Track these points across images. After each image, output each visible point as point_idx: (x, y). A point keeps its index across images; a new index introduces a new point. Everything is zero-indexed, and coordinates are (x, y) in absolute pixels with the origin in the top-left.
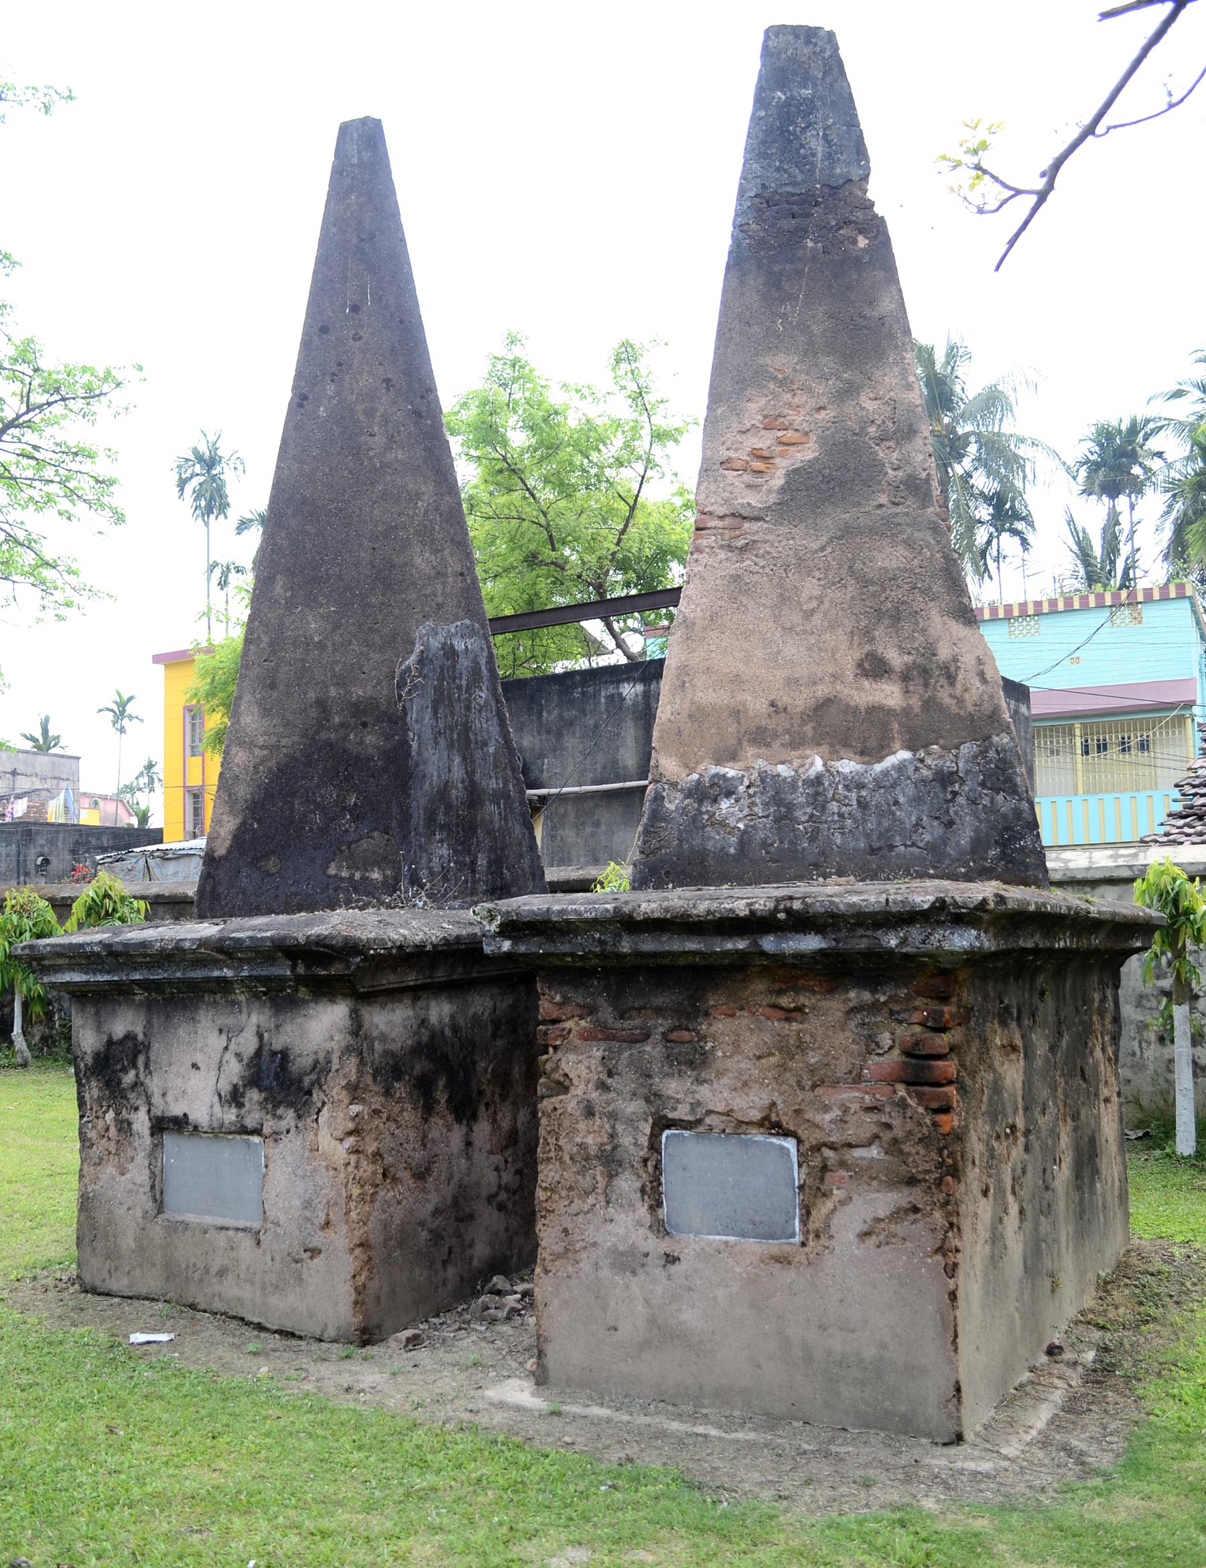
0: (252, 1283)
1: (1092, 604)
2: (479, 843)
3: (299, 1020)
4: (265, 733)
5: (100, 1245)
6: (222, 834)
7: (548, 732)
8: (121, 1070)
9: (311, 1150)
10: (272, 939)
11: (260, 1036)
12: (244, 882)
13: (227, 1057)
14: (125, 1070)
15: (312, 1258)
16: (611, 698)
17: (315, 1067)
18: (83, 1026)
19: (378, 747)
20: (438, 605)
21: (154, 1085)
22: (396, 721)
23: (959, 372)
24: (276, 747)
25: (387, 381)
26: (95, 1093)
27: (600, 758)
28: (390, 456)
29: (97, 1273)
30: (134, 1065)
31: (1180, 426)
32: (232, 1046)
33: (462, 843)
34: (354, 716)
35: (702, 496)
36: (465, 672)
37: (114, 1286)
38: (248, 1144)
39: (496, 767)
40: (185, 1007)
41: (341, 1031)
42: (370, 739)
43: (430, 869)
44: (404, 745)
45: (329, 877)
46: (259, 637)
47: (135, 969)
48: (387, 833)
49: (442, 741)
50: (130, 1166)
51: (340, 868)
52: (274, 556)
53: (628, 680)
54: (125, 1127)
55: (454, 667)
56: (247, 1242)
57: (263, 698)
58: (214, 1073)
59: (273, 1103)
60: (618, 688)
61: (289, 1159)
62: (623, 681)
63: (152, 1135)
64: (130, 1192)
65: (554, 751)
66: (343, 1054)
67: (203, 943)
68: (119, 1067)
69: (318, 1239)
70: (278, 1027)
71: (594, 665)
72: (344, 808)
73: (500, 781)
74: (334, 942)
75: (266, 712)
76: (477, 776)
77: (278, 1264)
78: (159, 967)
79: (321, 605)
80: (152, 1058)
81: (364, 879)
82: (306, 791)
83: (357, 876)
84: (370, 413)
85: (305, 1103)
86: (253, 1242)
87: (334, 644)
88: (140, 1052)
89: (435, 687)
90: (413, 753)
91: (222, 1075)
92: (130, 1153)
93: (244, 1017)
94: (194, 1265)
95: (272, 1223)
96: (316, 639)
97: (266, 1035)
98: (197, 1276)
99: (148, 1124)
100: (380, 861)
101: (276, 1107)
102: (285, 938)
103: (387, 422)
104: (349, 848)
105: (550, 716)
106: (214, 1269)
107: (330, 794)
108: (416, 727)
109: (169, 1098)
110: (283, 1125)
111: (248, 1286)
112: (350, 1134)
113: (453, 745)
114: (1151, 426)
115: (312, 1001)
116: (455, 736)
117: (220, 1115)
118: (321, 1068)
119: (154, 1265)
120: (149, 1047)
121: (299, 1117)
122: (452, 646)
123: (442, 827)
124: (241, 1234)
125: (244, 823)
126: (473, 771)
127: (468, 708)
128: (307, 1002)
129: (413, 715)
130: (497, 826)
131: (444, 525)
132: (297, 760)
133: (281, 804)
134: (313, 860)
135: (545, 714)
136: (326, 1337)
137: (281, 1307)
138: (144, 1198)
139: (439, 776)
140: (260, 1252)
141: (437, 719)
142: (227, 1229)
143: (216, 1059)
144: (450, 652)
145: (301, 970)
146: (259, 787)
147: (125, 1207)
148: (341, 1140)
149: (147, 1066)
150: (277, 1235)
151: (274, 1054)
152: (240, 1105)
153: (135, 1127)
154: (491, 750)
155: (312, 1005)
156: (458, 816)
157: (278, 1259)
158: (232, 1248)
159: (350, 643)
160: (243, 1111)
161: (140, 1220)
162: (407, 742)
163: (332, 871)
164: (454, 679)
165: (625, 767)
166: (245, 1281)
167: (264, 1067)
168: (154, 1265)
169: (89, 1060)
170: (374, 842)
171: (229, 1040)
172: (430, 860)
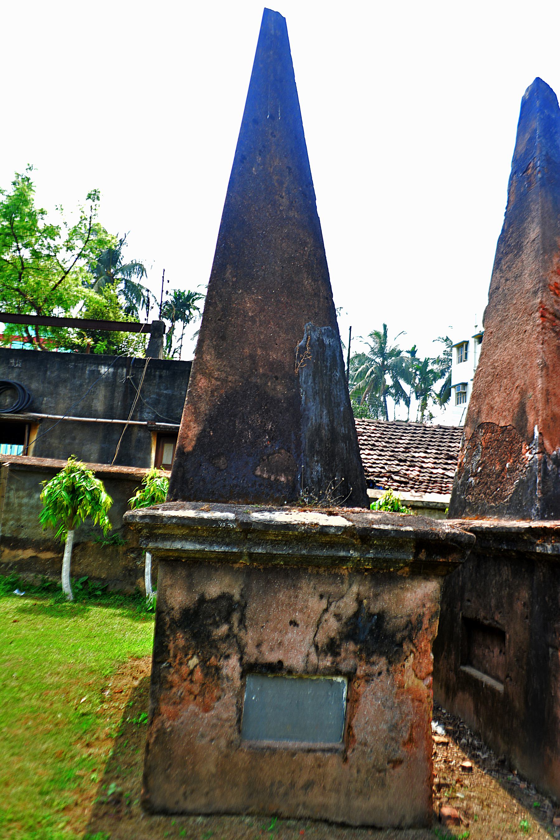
0: (338, 791)
2: (337, 466)
3: (396, 592)
4: (218, 370)
5: (175, 773)
6: (190, 435)
7: (49, 383)
10: (415, 533)
11: (359, 602)
12: (204, 473)
13: (326, 616)
14: (217, 625)
15: (394, 768)
16: (92, 372)
17: (407, 626)
18: (171, 586)
19: (283, 394)
20: (316, 313)
21: (249, 638)
22: (294, 380)
23: (122, 251)
24: (224, 381)
25: (289, 168)
26: (181, 642)
27: (81, 403)
28: (291, 214)
29: (168, 792)
30: (227, 620)
32: (332, 608)
33: (328, 465)
34: (271, 371)
35: (544, 299)
36: (329, 358)
37: (189, 806)
38: (332, 683)
39: (344, 420)
40: (287, 576)
41: (431, 601)
43: (312, 478)
44: (298, 395)
45: (256, 476)
46: (215, 303)
48: (289, 452)
49: (317, 398)
50: (216, 704)
51: (262, 471)
52: (226, 252)
53: (105, 365)
54: (213, 673)
55: (324, 353)
56: (334, 761)
57: (217, 345)
59: (366, 653)
60: (98, 367)
62: (102, 364)
64: (214, 726)
65: (52, 394)
70: (376, 596)
71: (12, 348)
72: (265, 430)
73: (346, 429)
77: (363, 775)
78: (285, 544)
79: (253, 293)
82: (243, 414)
83: (273, 478)
84: (281, 183)
86: (341, 759)
87: (260, 321)
88: (234, 610)
89: (314, 363)
90: (303, 402)
91: (321, 631)
92: (216, 693)
93: (345, 587)
94: (280, 782)
95: (360, 743)
96: (250, 314)
97: (365, 601)
98: (282, 790)
99: (238, 669)
100: (286, 470)
101: (369, 655)
103: (289, 193)
104: (268, 457)
105: (52, 374)
106: (301, 782)
107: (256, 419)
109: (264, 648)
110: (376, 668)
111: (333, 794)
113: (323, 402)
114: (197, 296)
115: (408, 578)
116: (324, 397)
117: (315, 661)
118: (413, 627)
121: (390, 663)
122: (323, 340)
123: (318, 453)
124: (328, 755)
125: (204, 430)
126: (333, 421)
127: (330, 380)
130: (345, 457)
131: (318, 266)
132: (238, 393)
133: (227, 421)
134: (247, 463)
135: (48, 373)
136: (403, 824)
138: (230, 731)
139: (316, 420)
140: (346, 767)
141: (315, 384)
143: (315, 618)
146: (214, 406)
147: (208, 739)
150: (364, 753)
151: (371, 615)
153: (224, 672)
154: (342, 409)
156: (326, 447)
158: (319, 766)
159: (269, 323)
160: (339, 659)
164: (324, 361)
165: (96, 410)
167: (361, 625)
169: (177, 615)
170: (281, 457)
171: (329, 604)
172: (312, 473)
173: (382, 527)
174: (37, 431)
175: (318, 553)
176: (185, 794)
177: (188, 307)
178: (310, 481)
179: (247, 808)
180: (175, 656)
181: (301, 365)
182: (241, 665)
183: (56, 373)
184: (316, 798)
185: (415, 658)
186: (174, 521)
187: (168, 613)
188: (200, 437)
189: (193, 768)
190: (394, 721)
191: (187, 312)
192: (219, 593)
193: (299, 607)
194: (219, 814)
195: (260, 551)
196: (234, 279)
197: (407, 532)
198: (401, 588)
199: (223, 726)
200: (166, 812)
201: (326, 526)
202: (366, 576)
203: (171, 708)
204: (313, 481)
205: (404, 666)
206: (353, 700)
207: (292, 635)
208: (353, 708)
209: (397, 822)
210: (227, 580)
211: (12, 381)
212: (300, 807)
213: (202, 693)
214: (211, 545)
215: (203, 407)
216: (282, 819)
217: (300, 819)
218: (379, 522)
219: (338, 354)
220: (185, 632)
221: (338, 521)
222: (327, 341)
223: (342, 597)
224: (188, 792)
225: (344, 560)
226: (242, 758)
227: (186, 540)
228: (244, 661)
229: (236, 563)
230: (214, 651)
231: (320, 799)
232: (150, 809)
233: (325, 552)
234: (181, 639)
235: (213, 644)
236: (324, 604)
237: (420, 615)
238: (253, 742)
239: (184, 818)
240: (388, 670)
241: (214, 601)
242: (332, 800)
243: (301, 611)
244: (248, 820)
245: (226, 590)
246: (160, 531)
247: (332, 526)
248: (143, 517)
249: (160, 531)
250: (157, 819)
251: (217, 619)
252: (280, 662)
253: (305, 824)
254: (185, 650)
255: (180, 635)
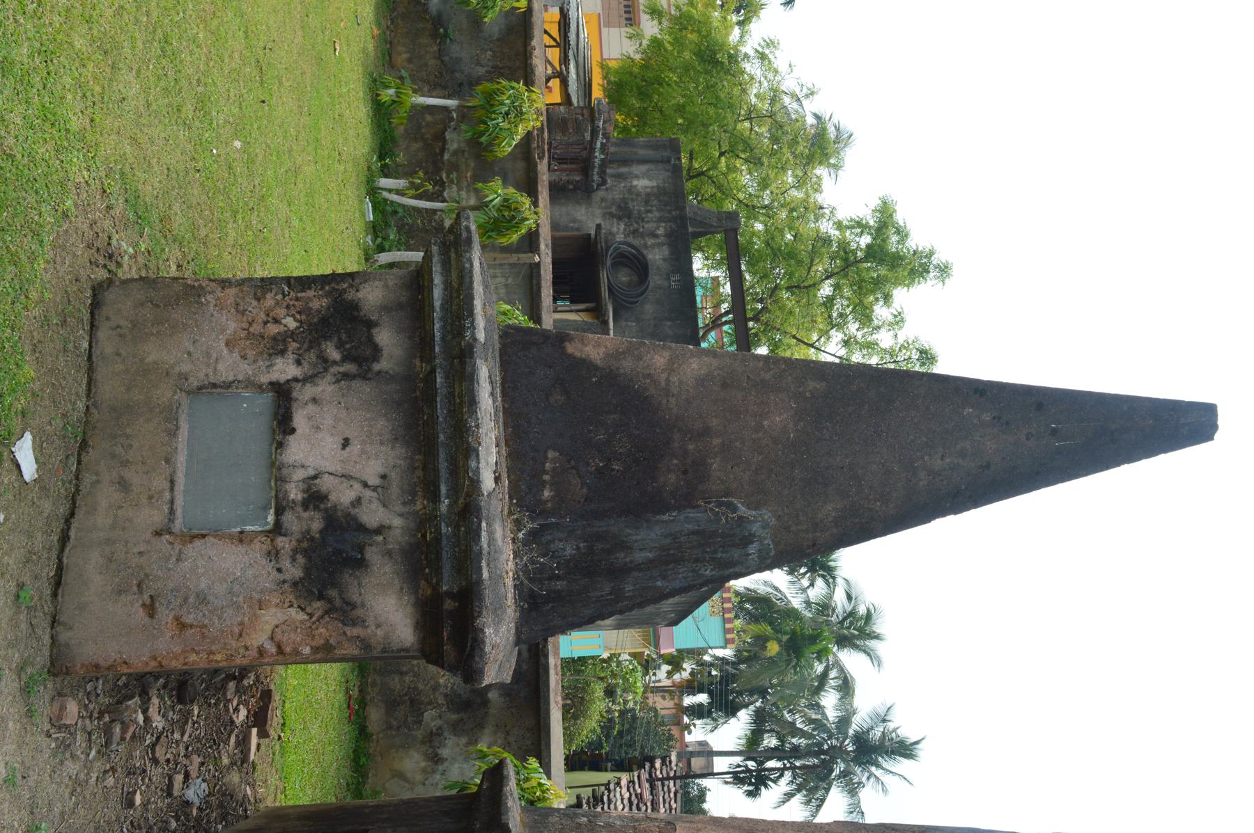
0: (113, 527)
1: (729, 636)
4: (681, 382)
8: (340, 339)
9: (260, 601)
10: (480, 581)
11: (380, 530)
13: (357, 486)
14: (340, 346)
15: (144, 605)
17: (348, 604)
21: (325, 387)
22: (687, 499)
24: (667, 393)
26: (315, 305)
29: (120, 307)
30: (346, 358)
31: (830, 596)
32: (368, 493)
37: (102, 334)
38: (266, 508)
41: (386, 637)
42: (672, 477)
43: (553, 541)
44: (666, 508)
45: (546, 452)
47: (447, 377)
49: (668, 541)
50: (236, 355)
51: (554, 460)
54: (277, 347)
56: (156, 517)
58: (337, 468)
59: (309, 548)
61: (250, 572)
63: (271, 383)
64: (208, 355)
66: (362, 640)
67: (476, 483)
68: (344, 337)
69: (165, 615)
70: (389, 553)
74: (477, 659)
75: (701, 381)
76: (635, 574)
78: (450, 411)
80: (353, 383)
81: (544, 483)
83: (546, 477)
85: (310, 592)
88: (360, 366)
91: (337, 480)
92: (251, 354)
93: (399, 508)
97: (380, 538)
98: (119, 450)
99: (283, 378)
101: (306, 553)
102: (481, 599)
104: (573, 468)
106: (129, 474)
108: (682, 517)
109: (311, 408)
110: (286, 564)
111: (110, 521)
112: (279, 647)
117: (295, 478)
119: (128, 390)
120: (365, 378)
121: (295, 584)
122: (752, 542)
124: (166, 508)
125: (596, 368)
127: (697, 560)
128: (416, 592)
129: (692, 514)
133: (614, 401)
135: (669, 323)
136: (59, 628)
137: (90, 569)
139: (636, 541)
140: (148, 535)
142: (172, 489)
143: (354, 471)
144: (747, 541)
145: (449, 605)
147: (191, 349)
148: (272, 638)
149: (346, 376)
150: (168, 559)
151: (361, 549)
152: (306, 505)
153: (279, 361)
154: (659, 583)
155: (413, 599)
157: (142, 561)
158: (150, 498)
160: (299, 509)
161: (177, 369)
162: (668, 510)
163: (551, 454)
166: (116, 516)
168: (128, 390)
169: (350, 296)
171: (375, 489)
172: (560, 540)
173: (484, 534)
174: (590, 320)
175: (442, 456)
176: (118, 327)
177: (812, 569)
178: (549, 538)
179: (96, 407)
180: (297, 299)
181: (712, 510)
182: (288, 381)
183: (670, 333)
184: (106, 496)
185: (302, 622)
186: (467, 265)
187: (351, 286)
188: (585, 364)
189: (152, 334)
190: (211, 598)
191: (803, 570)
192: (381, 344)
193: (368, 448)
194: (91, 370)
195: (438, 380)
196: (808, 395)
197: (480, 568)
198: (402, 589)
199: (208, 365)
200: (95, 305)
201: (478, 455)
202: (415, 536)
203: (231, 300)
204: (549, 542)
205: (291, 606)
206: (242, 538)
207: (330, 443)
208: (231, 537)
209: (62, 618)
210: (398, 352)
211: (650, 278)
212: (94, 478)
213: (250, 336)
214: (441, 319)
215: (627, 365)
216: (79, 455)
217: (77, 478)
218: (491, 534)
219: (737, 569)
220: (328, 309)
221: (488, 482)
222: (752, 549)
223: (384, 506)
224: (122, 332)
225: (435, 497)
226: (164, 393)
227: (445, 289)
228: (294, 384)
229: (422, 361)
230: (305, 346)
231: (104, 504)
232: (98, 290)
233: (443, 465)
234: (318, 302)
235: (314, 344)
236: (374, 481)
237: (364, 621)
238: (185, 408)
239: (87, 328)
240: (284, 582)
241: (370, 339)
242: (102, 519)
243: (363, 451)
244: (81, 405)
245: (385, 353)
246: (453, 255)
247: (479, 463)
248: (468, 229)
249: (453, 255)
250: (89, 293)
251: (348, 346)
252: (293, 431)
253: (70, 482)
254: (306, 310)
255: (325, 302)
